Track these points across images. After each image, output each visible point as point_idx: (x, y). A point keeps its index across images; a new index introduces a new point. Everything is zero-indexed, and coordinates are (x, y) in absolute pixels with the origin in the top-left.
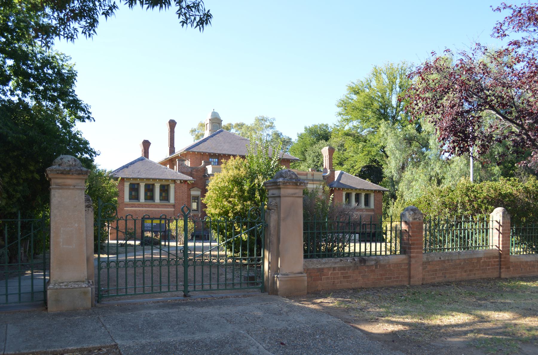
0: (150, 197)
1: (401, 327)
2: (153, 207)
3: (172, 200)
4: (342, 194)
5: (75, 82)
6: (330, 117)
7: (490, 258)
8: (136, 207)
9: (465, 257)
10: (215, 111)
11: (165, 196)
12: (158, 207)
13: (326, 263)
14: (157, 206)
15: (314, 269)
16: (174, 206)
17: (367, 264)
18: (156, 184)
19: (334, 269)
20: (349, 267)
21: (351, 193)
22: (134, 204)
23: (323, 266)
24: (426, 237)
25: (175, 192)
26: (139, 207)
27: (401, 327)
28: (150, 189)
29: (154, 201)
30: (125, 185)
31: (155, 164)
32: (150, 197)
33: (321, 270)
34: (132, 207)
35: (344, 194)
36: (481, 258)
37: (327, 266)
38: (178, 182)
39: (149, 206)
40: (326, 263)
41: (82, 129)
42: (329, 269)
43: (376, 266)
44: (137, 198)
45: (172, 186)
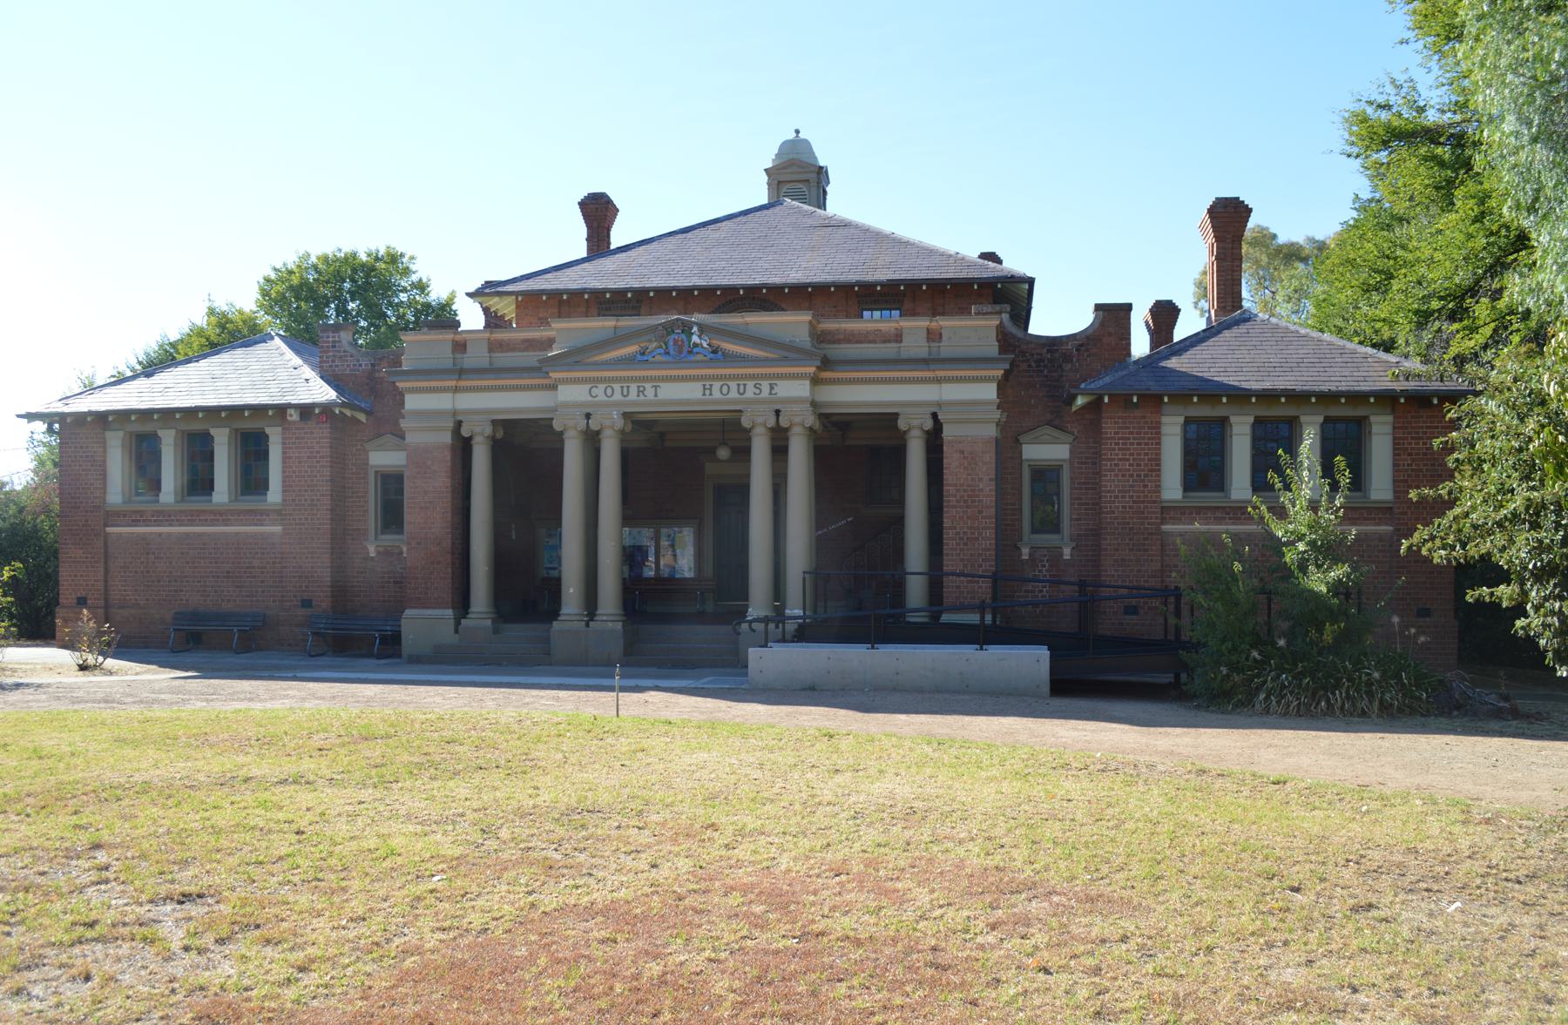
0: (199, 482)
2: (205, 523)
3: (274, 495)
4: (1157, 427)
5: (1348, 149)
8: (147, 523)
11: (252, 480)
12: (226, 523)
14: (220, 516)
16: (279, 514)
18: (1233, 419)
21: (1223, 422)
22: (141, 513)
24: (263, 805)
25: (285, 459)
26: (158, 523)
28: (198, 450)
30: (1165, 430)
31: (1148, 357)
32: (199, 482)
34: (135, 523)
38: (293, 416)
39: (193, 518)
44: (156, 485)
45: (275, 435)
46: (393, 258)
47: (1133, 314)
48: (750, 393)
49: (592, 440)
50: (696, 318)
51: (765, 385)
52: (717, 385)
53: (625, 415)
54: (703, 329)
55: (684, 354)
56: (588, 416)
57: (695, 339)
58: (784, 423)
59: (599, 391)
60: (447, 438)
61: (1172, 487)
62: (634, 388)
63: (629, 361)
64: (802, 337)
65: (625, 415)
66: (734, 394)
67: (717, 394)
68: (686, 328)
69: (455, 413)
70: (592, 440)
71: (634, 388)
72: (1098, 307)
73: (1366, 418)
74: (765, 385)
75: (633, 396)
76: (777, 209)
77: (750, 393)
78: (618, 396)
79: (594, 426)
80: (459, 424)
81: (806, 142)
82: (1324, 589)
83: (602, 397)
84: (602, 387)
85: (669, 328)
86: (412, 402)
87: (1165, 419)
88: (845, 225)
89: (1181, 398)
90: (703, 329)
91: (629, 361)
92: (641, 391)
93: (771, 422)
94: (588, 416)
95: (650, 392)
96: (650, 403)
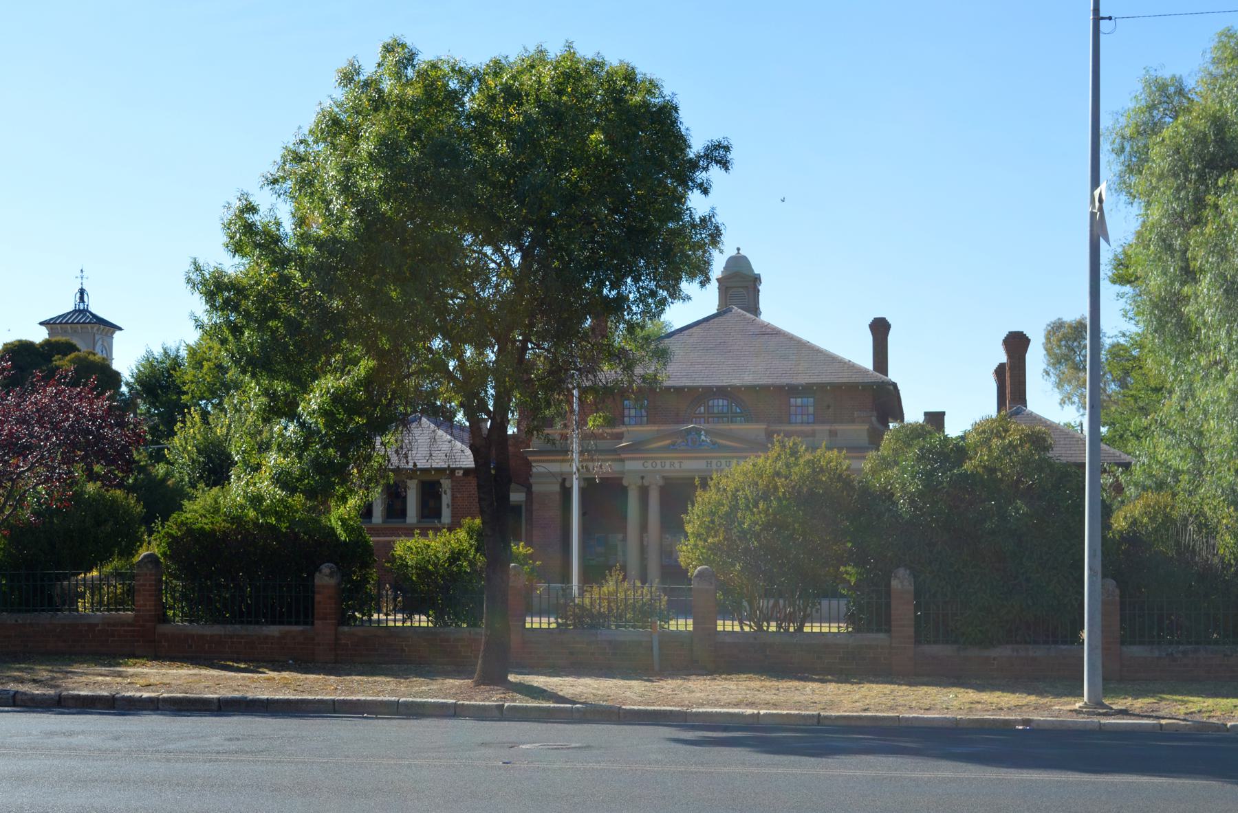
7: (109, 625)
36: (97, 625)
44: (403, 514)
45: (446, 483)
47: (946, 418)
53: (664, 477)
54: (707, 433)
56: (642, 478)
59: (649, 465)
60: (557, 488)
65: (664, 477)
69: (561, 474)
70: (644, 492)
72: (926, 414)
73: (1124, 556)
75: (667, 467)
76: (728, 316)
78: (659, 467)
79: (646, 483)
80: (564, 480)
81: (745, 258)
82: (424, 420)
83: (650, 467)
85: (689, 431)
86: (538, 468)
88: (776, 333)
91: (666, 449)
92: (672, 465)
93: (639, 483)
94: (642, 478)
95: (677, 466)
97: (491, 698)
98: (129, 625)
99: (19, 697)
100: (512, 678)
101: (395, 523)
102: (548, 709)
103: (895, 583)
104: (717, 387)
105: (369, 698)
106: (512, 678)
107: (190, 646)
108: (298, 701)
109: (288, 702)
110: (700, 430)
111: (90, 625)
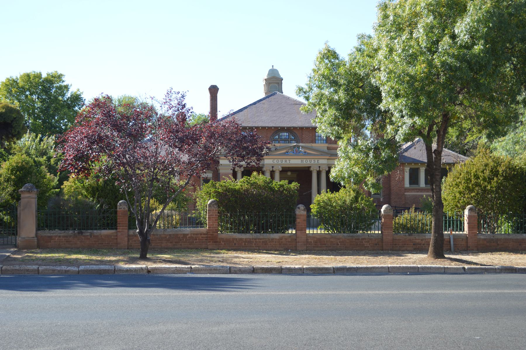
1: (202, 266)
6: (88, 98)
7: (194, 234)
9: (171, 233)
10: (275, 68)
13: (54, 233)
14: (422, 190)
15: (45, 236)
17: (84, 234)
18: (421, 168)
19: (59, 237)
20: (70, 236)
23: (52, 235)
27: (202, 266)
29: (419, 186)
33: (50, 237)
35: (407, 170)
36: (188, 235)
37: (54, 235)
40: (54, 233)
41: (44, 76)
42: (56, 236)
43: (91, 236)
46: (59, 77)
48: (313, 162)
49: (319, 173)
50: (301, 144)
51: (316, 160)
52: (304, 160)
55: (298, 153)
56: (273, 167)
57: (300, 149)
58: (321, 169)
59: (275, 161)
61: (407, 184)
62: (284, 160)
63: (284, 154)
64: (325, 149)
66: (309, 162)
67: (304, 162)
68: (299, 147)
70: (319, 173)
71: (284, 160)
74: (316, 160)
75: (284, 162)
77: (313, 162)
78: (280, 162)
79: (274, 169)
81: (276, 70)
83: (276, 162)
84: (276, 160)
85: (294, 147)
87: (405, 168)
89: (410, 164)
90: (303, 147)
91: (284, 154)
92: (286, 161)
94: (273, 167)
95: (288, 162)
96: (288, 164)
97: (439, 264)
98: (204, 234)
99: (232, 269)
100: (446, 256)
101: (414, 186)
102: (475, 269)
103: (298, 212)
104: (287, 127)
105: (437, 266)
106: (446, 256)
107: (235, 244)
108: (371, 268)
109: (367, 268)
110: (300, 146)
111: (184, 234)
